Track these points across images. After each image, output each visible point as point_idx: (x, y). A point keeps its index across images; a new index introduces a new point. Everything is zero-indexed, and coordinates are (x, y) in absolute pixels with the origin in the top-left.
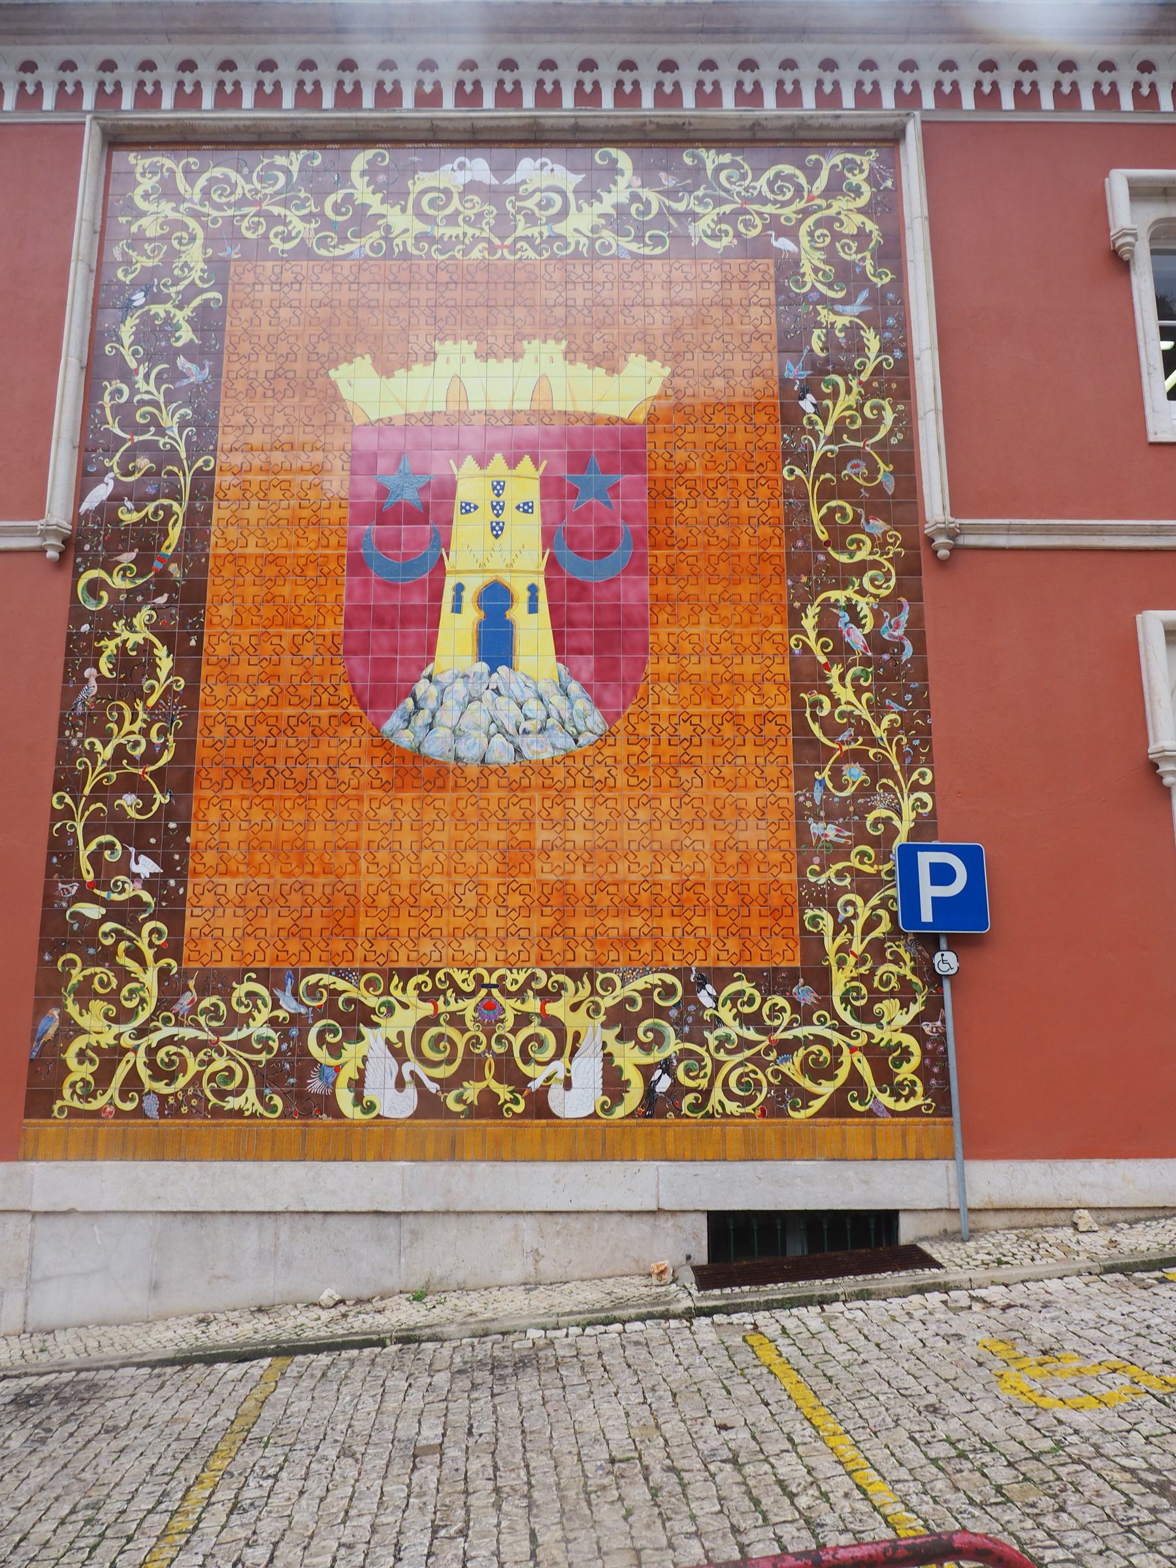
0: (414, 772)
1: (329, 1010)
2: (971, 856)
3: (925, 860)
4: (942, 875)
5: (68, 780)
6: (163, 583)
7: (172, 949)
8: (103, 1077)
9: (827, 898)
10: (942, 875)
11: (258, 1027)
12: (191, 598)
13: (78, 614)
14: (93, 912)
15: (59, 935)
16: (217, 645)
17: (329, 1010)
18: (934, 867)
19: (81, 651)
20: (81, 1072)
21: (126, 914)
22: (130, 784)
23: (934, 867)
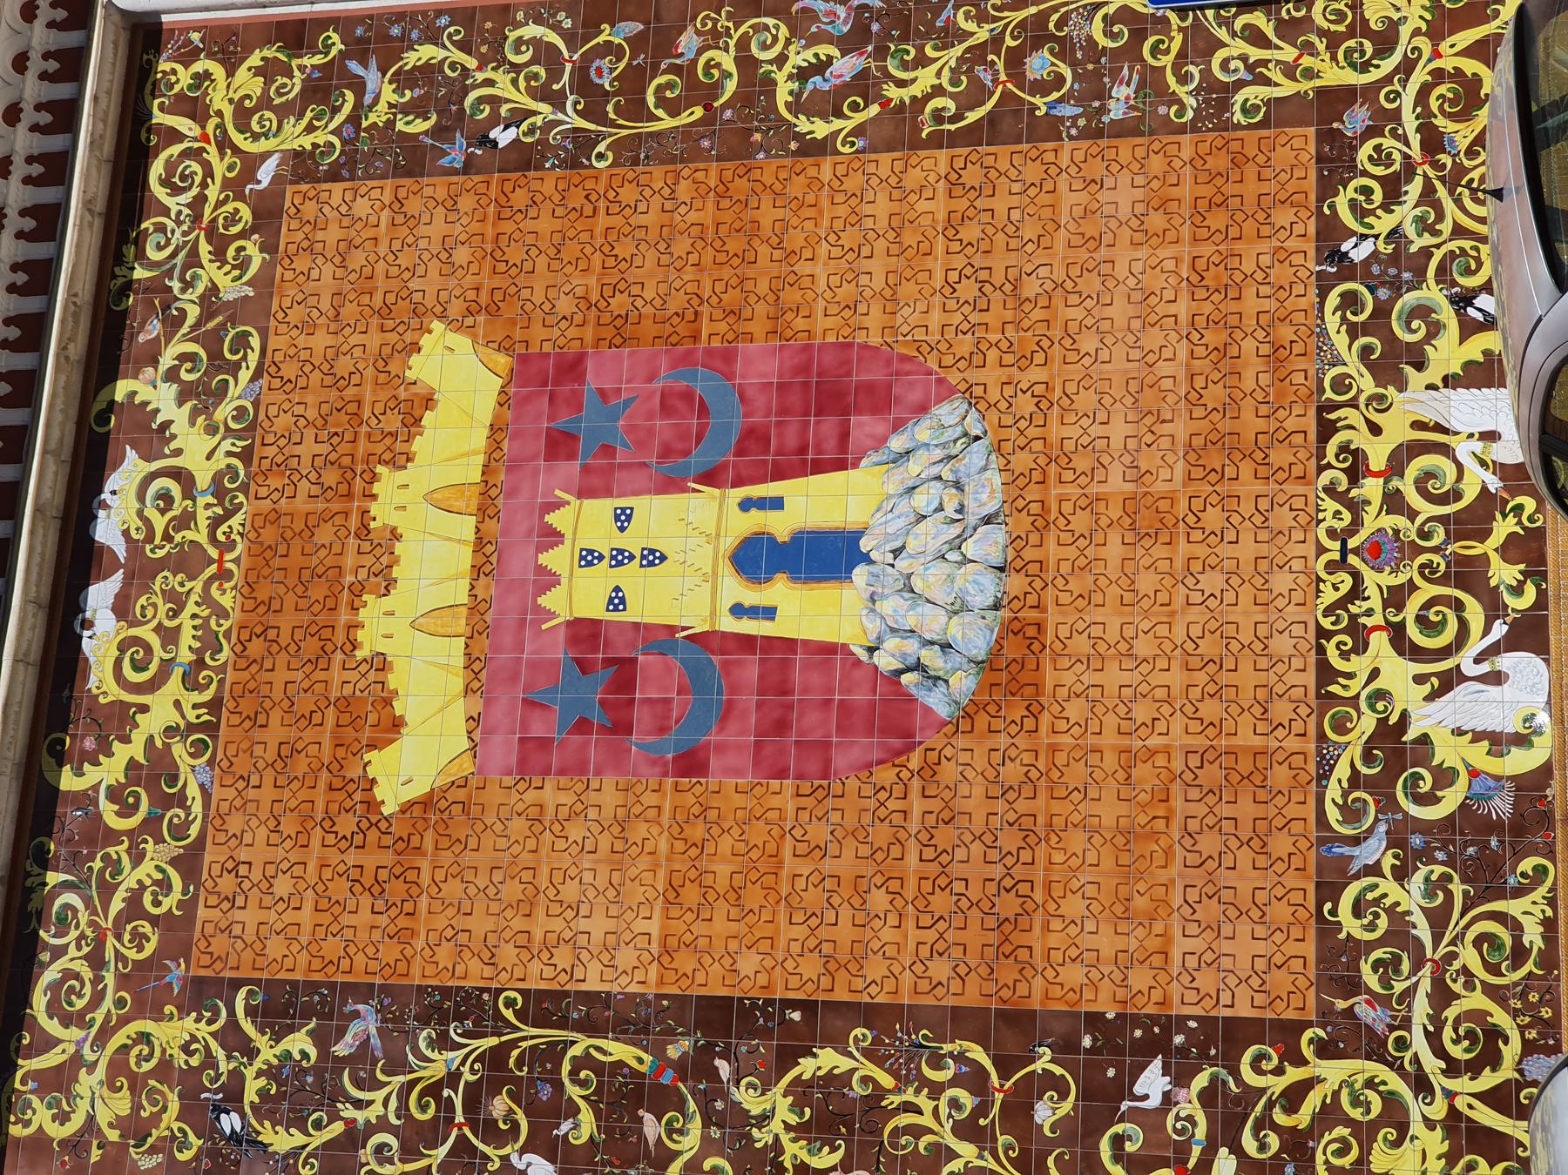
0: (1016, 665)
1: (1381, 788)
6: (698, 1067)
9: (1217, 96)
11: (1411, 897)
12: (721, 1019)
16: (801, 977)
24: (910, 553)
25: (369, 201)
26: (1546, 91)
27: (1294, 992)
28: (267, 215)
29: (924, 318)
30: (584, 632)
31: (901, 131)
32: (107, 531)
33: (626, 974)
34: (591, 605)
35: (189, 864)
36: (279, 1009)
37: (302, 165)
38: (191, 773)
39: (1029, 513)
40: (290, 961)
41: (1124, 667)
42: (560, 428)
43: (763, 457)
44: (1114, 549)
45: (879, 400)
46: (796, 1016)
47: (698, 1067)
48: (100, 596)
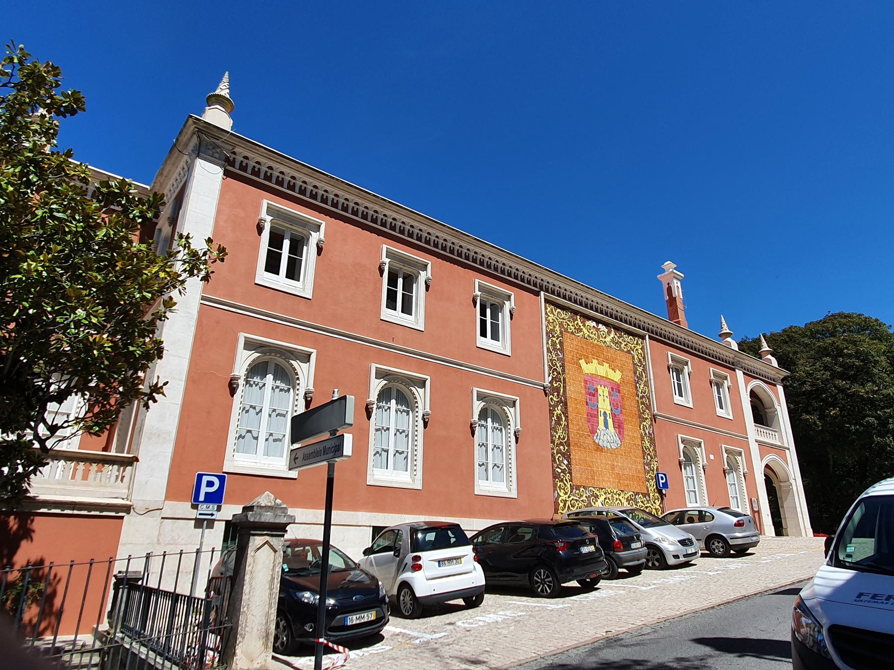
0: (599, 448)
1: (593, 495)
2: (665, 475)
3: (205, 479)
4: (210, 484)
5: (553, 442)
6: (562, 402)
7: (571, 480)
8: (565, 506)
9: (648, 480)
10: (210, 484)
11: (584, 498)
12: (565, 404)
13: (550, 405)
14: (560, 471)
15: (556, 476)
16: (570, 417)
17: (593, 495)
18: (208, 482)
19: (551, 413)
20: (562, 505)
21: (563, 471)
22: (561, 444)
23: (208, 482)
24: (607, 436)
25: (631, 366)
26: (322, 513)
27: (576, 482)
28: (629, 352)
29: (627, 440)
30: (597, 390)
31: (642, 439)
32: (600, 325)
33: (568, 393)
34: (600, 392)
35: (572, 333)
36: (561, 343)
37: (633, 357)
38: (580, 334)
39: (612, 452)
40: (565, 344)
41: (601, 462)
42: (615, 389)
43: (614, 416)
45: (620, 432)
46: (732, 552)
47: (562, 402)
48: (594, 324)
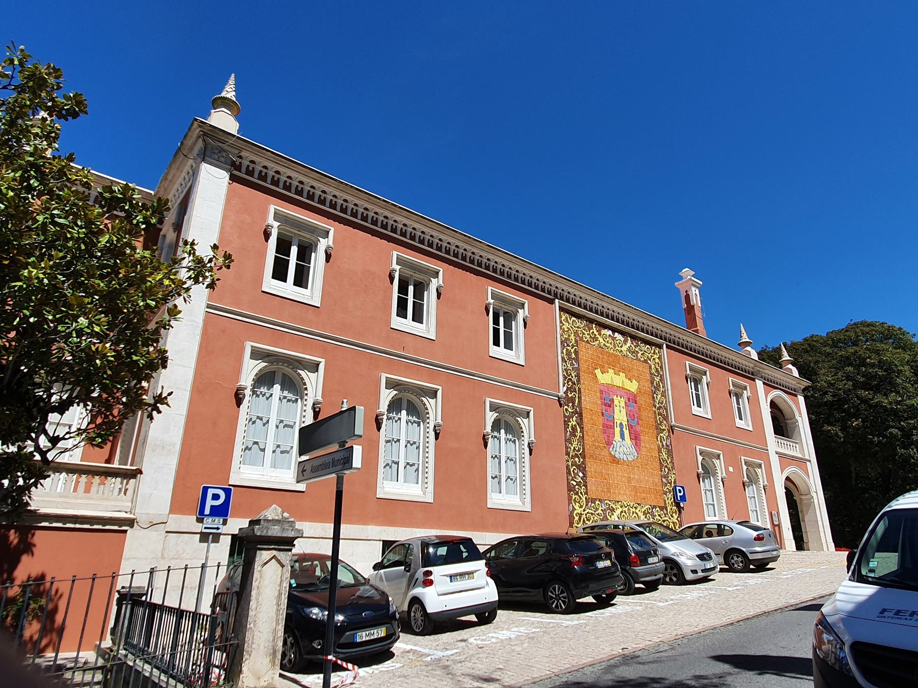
0: (615, 460)
1: (608, 509)
2: (683, 488)
3: (211, 492)
4: (216, 497)
5: (568, 454)
6: (577, 413)
7: (586, 493)
8: (580, 519)
9: (665, 493)
10: (216, 497)
11: (600, 511)
12: (581, 415)
13: (565, 416)
14: (575, 483)
15: (570, 489)
16: (586, 429)
17: (608, 509)
18: (214, 495)
19: (566, 424)
20: (577, 518)
21: (578, 484)
22: (576, 456)
23: (214, 495)
24: (623, 447)
25: (648, 376)
27: (592, 495)
28: (645, 361)
29: (644, 451)
30: (613, 401)
31: (660, 451)
32: (616, 334)
33: (584, 404)
34: (616, 402)
35: (587, 342)
36: (576, 352)
37: (650, 367)
38: (596, 343)
39: (628, 464)
40: (581, 353)
41: (617, 475)
42: (632, 399)
43: (630, 427)
44: (34, 273)
45: (636, 444)
46: (752, 567)
47: (577, 413)
48: (610, 332)
